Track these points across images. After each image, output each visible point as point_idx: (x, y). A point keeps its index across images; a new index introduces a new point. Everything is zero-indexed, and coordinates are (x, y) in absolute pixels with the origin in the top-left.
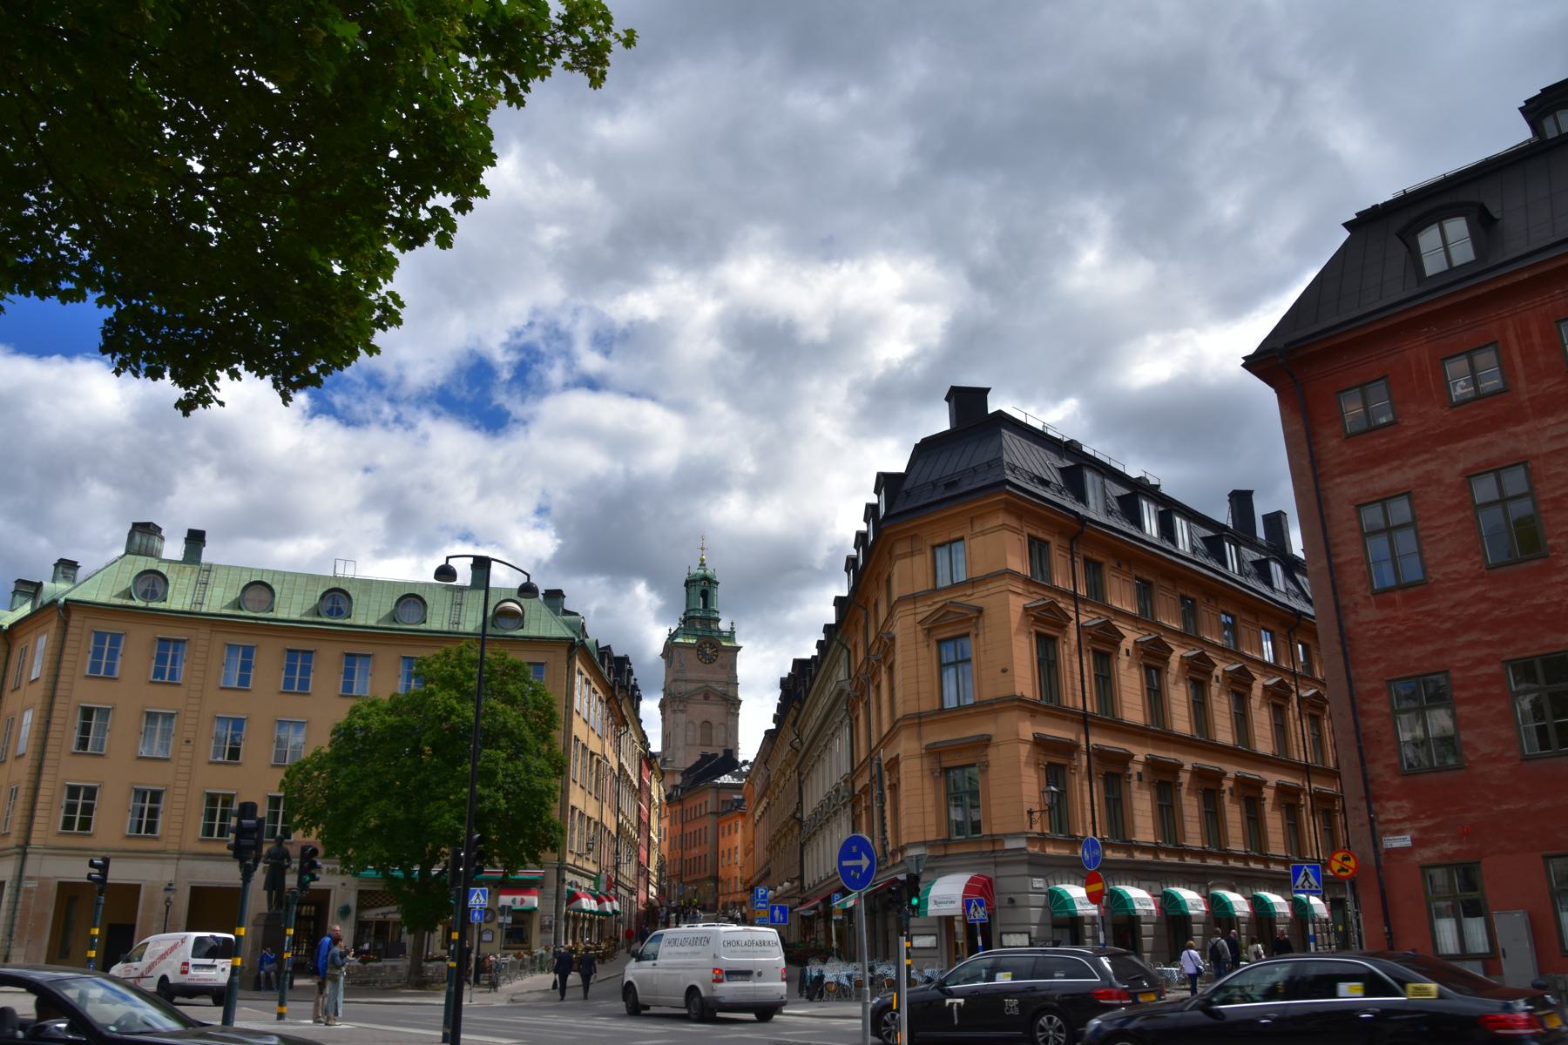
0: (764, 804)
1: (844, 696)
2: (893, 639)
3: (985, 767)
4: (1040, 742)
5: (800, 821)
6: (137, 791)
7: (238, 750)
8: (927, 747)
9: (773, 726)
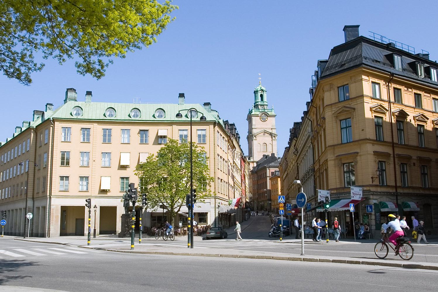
0: (286, 173)
3: (356, 162)
4: (376, 153)
9: (288, 146)
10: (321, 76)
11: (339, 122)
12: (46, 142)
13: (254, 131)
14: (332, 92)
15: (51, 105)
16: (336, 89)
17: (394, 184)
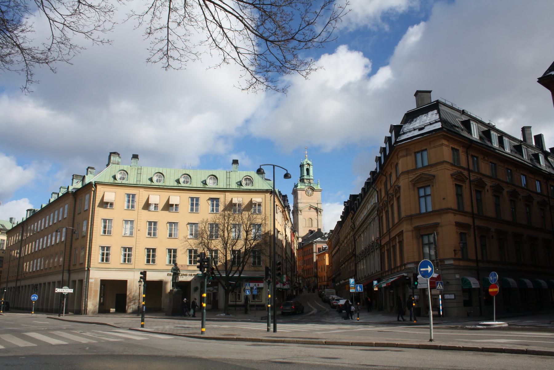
1: (376, 208)
2: (399, 187)
4: (458, 224)
5: (355, 255)
6: (148, 249)
7: (111, 231)
8: (414, 228)
9: (341, 220)
10: (396, 140)
11: (416, 190)
12: (86, 208)
13: (300, 205)
14: (409, 158)
15: (93, 168)
16: (413, 155)
17: (474, 258)
